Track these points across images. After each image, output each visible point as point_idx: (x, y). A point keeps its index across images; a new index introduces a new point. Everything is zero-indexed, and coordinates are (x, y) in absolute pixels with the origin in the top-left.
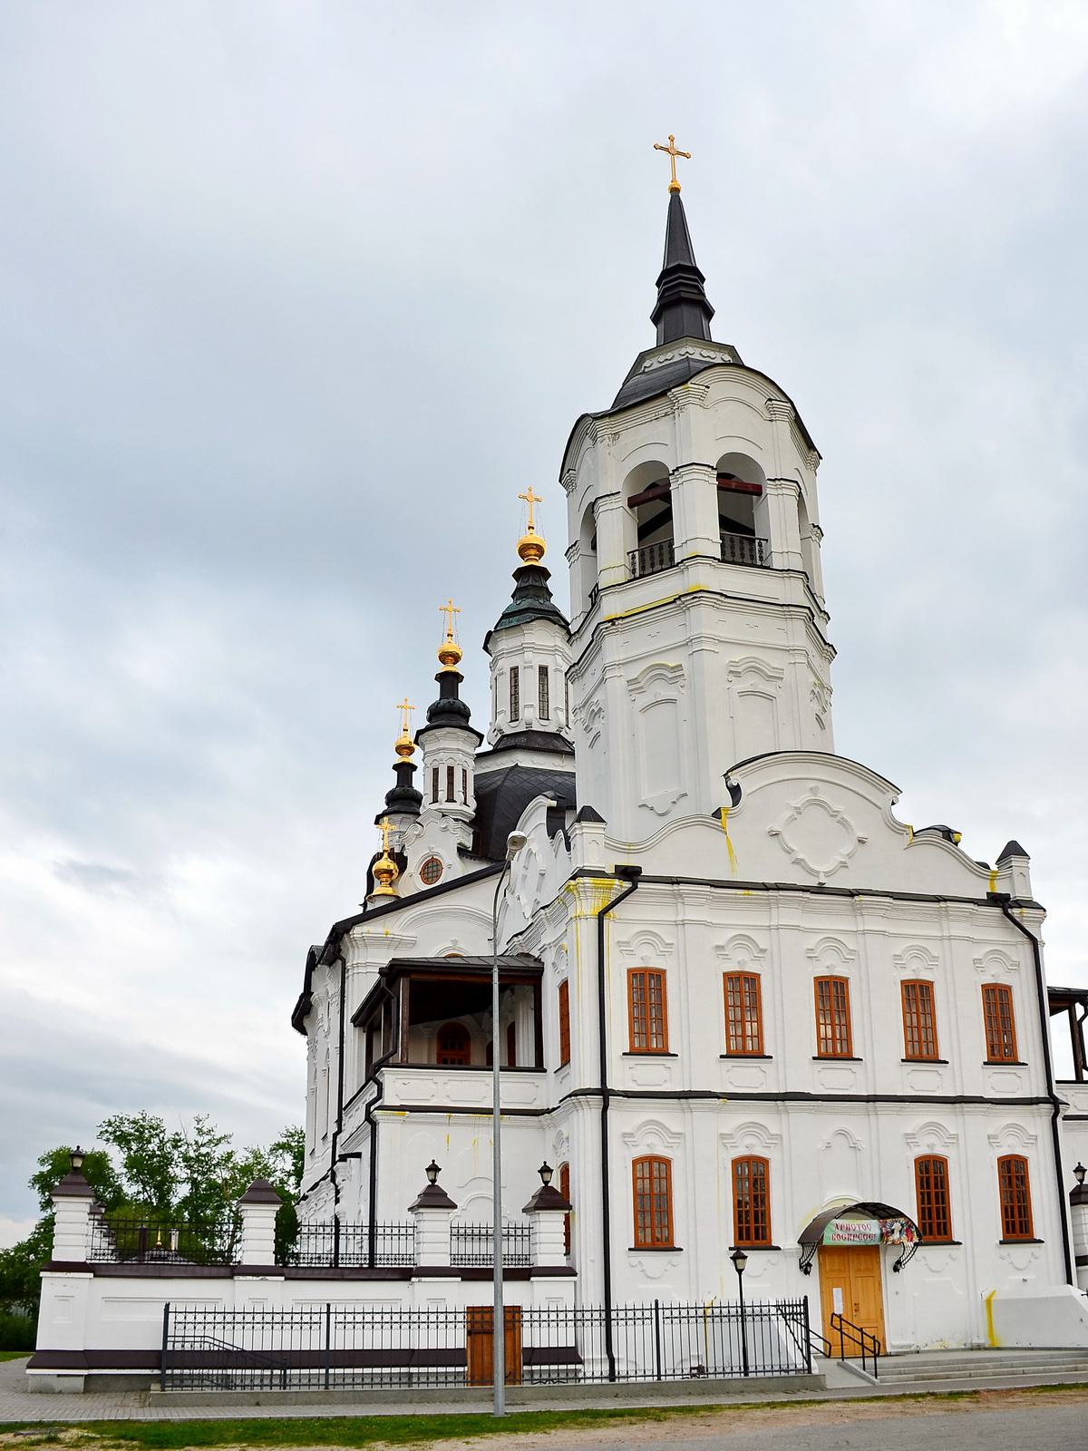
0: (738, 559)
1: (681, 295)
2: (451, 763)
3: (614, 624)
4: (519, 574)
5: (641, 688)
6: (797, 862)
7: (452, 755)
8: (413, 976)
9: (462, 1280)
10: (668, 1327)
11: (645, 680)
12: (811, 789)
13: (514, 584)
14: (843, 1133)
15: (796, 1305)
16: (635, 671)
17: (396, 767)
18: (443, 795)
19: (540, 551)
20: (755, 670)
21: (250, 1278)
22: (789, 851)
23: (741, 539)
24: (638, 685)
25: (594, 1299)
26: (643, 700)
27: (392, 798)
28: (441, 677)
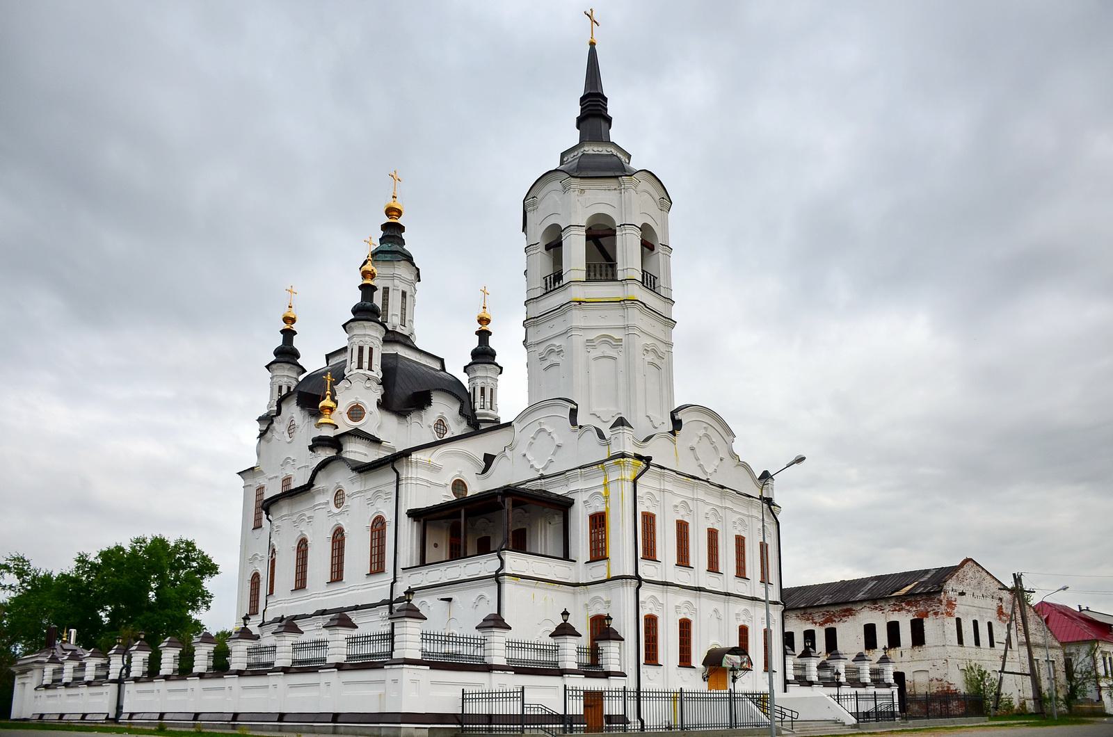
0: (598, 276)
1: (594, 111)
2: (361, 344)
3: (580, 304)
4: (385, 227)
6: (700, 466)
7: (373, 340)
8: (514, 497)
9: (586, 677)
10: (571, 701)
12: (705, 428)
16: (593, 335)
17: (283, 332)
18: (366, 365)
19: (400, 213)
20: (654, 351)
21: (499, 672)
22: (697, 459)
25: (632, 686)
26: (594, 353)
27: (278, 352)
28: (479, 333)
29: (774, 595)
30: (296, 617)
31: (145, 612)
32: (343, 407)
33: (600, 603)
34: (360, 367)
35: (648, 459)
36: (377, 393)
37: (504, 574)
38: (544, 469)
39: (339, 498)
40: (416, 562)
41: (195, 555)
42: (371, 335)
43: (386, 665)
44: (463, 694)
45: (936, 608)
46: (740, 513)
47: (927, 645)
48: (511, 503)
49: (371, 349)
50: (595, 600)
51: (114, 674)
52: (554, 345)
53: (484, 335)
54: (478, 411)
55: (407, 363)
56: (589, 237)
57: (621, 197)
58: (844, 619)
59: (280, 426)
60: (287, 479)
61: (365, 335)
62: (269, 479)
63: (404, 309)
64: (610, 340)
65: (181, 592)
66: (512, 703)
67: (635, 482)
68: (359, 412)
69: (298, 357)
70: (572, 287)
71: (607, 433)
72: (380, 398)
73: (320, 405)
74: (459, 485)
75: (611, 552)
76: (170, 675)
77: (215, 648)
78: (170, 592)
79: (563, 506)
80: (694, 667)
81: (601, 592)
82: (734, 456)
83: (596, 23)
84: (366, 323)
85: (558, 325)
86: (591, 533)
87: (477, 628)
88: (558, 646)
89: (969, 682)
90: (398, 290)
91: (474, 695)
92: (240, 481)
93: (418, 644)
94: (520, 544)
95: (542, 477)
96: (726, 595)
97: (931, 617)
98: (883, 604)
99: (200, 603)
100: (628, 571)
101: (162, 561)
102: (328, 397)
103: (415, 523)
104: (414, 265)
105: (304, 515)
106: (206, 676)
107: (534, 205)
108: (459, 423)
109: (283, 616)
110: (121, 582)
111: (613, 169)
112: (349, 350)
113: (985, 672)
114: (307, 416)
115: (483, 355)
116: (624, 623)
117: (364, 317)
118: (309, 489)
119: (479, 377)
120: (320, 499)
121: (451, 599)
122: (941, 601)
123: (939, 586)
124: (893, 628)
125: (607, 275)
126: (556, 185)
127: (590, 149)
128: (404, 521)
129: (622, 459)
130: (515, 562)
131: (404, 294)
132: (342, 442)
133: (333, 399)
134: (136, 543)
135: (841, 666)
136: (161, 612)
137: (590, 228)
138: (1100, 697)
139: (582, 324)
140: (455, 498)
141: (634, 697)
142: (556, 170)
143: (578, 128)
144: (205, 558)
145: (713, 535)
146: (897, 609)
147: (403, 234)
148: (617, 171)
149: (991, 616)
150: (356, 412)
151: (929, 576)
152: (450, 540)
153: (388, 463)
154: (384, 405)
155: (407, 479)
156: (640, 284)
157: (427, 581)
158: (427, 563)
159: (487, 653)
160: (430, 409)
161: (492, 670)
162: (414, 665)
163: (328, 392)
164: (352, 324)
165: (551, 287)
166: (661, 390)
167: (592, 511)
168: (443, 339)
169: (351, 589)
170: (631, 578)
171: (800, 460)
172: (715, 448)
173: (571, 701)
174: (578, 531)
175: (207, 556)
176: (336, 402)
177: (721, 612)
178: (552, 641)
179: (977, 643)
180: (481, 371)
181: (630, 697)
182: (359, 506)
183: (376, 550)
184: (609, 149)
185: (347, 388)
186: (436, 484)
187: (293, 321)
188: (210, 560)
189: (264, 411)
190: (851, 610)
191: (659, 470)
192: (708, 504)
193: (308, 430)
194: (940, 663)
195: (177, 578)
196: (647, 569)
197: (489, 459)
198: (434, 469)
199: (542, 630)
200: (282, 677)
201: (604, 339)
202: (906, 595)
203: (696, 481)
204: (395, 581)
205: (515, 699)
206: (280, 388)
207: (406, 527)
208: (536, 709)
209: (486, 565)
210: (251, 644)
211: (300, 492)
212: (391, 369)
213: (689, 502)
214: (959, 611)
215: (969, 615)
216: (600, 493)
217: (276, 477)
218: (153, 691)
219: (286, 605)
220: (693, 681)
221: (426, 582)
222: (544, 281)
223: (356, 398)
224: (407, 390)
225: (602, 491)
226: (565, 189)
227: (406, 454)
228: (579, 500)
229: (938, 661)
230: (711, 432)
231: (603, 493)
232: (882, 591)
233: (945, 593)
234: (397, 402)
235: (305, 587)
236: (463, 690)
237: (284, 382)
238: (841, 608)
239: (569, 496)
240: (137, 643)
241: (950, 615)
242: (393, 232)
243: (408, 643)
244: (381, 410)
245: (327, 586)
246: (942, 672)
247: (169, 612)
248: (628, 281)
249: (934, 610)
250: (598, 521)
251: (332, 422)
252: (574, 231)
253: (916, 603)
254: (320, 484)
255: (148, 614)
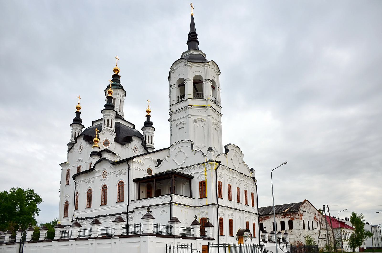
0: (197, 97)
1: (193, 39)
2: (108, 118)
3: (192, 107)
4: (113, 76)
5: (196, 122)
6: (234, 165)
7: (108, 116)
8: (175, 175)
9: (203, 240)
11: (198, 120)
13: (112, 78)
14: (248, 216)
15: (236, 245)
16: (196, 118)
17: (76, 112)
18: (110, 126)
19: (119, 71)
20: (216, 125)
21: (177, 238)
23: (198, 93)
24: (196, 121)
27: (74, 120)
29: (255, 211)
30: (99, 216)
31: (16, 216)
32: (102, 140)
33: (204, 213)
34: (108, 126)
35: (220, 162)
36: (114, 136)
37: (173, 203)
38: (181, 165)
39: (105, 174)
40: (136, 198)
41: (34, 195)
42: (111, 115)
43: (141, 236)
44: (167, 246)
45: (297, 216)
46: (246, 182)
47: (294, 229)
48: (174, 177)
49: (111, 120)
50: (202, 212)
51: (18, 240)
52: (182, 121)
53: (148, 117)
54: (147, 144)
55: (123, 126)
56: (194, 84)
57: (205, 69)
58: (266, 220)
59: (76, 147)
60: (79, 167)
61: (109, 115)
62: (72, 167)
63: (120, 106)
64: (202, 120)
65: (30, 209)
66: (170, 250)
67: (216, 170)
68: (107, 143)
69: (82, 122)
70: (189, 100)
71: (205, 153)
72: (115, 138)
73: (94, 140)
74: (149, 171)
75: (208, 195)
76: (7, 243)
77: (47, 231)
78: (26, 209)
79: (190, 178)
80: (234, 236)
81: (204, 209)
82: (243, 162)
83: (193, 8)
84: (110, 111)
85: (183, 114)
86: (200, 188)
87: (168, 222)
88: (194, 229)
89: (307, 241)
90: (119, 99)
91: (182, 246)
92: (60, 167)
93: (77, 232)
94: (172, 191)
95: (181, 168)
96: (243, 211)
97: (295, 219)
98: (279, 215)
99: (35, 213)
100: (214, 202)
101: (23, 197)
102: (97, 137)
103: (136, 184)
104: (124, 90)
105: (90, 180)
106: (60, 240)
107: (173, 71)
108: (141, 148)
109: (82, 218)
110: (7, 205)
111: (201, 59)
112: (103, 120)
113: (312, 238)
114: (87, 144)
115: (148, 124)
116: (214, 221)
117: (109, 108)
118: (93, 171)
119: (147, 132)
120: (97, 175)
121: (151, 212)
122: (299, 214)
123: (298, 209)
124: (283, 223)
125: (196, 97)
126: (182, 64)
127: (193, 52)
128: (132, 183)
129: (212, 162)
130: (176, 198)
131: (121, 101)
132: (102, 154)
133: (98, 138)
134: (12, 190)
135: (267, 235)
136: (22, 216)
137: (194, 80)
138: (343, 246)
139: (192, 114)
140: (149, 176)
141: (217, 246)
142: (180, 59)
143: (187, 44)
144: (38, 196)
145: (238, 189)
146: (284, 217)
147: (120, 79)
148: (203, 60)
149: (312, 219)
150: (106, 143)
151: (293, 206)
152: (147, 190)
153: (125, 161)
154: (116, 140)
155: (132, 167)
156: (212, 101)
157: (134, 206)
158: (140, 199)
159: (173, 231)
160: (132, 142)
161: (175, 237)
162: (152, 236)
163: (97, 135)
164: (105, 111)
165: (180, 100)
166: (218, 138)
167: (200, 180)
168: (134, 117)
169: (110, 208)
170: (216, 204)
171: (285, 163)
172: (238, 159)
173: (169, 250)
174: (195, 188)
175: (38, 195)
176: (99, 139)
177: (241, 217)
178: (191, 227)
179: (309, 229)
180: (148, 130)
181: (211, 246)
182: (114, 177)
183: (104, 194)
184: (199, 53)
185: (103, 134)
186: (142, 170)
187: (80, 109)
188: (39, 197)
189: (69, 141)
190: (268, 217)
191: (223, 166)
192: (237, 179)
193: (88, 149)
194: (298, 235)
195: (28, 203)
196: (220, 202)
197: (159, 162)
198: (142, 164)
199: (184, 223)
200: (95, 240)
201: (200, 119)
202: (287, 212)
203: (234, 171)
204: (73, 216)
205: (170, 249)
206: (75, 133)
207: (132, 185)
208: (195, 251)
209: (165, 199)
210: (62, 230)
211: (89, 172)
212: (118, 129)
213: (231, 178)
214: (304, 217)
215: (307, 219)
216: (203, 174)
217: (75, 166)
218: (36, 246)
219: (83, 214)
220: (233, 241)
221: (141, 206)
222: (177, 98)
223: (106, 138)
224: (124, 136)
225: (204, 173)
226: (186, 66)
227: (132, 158)
228: (195, 176)
229: (298, 235)
230: (237, 154)
231: (204, 174)
232: (280, 210)
233: (300, 211)
234: (120, 140)
235: (91, 207)
236: (167, 245)
237: (77, 131)
238: (265, 216)
239: (191, 175)
240: (7, 231)
241: (301, 219)
242: (116, 78)
243: (149, 227)
244: (115, 142)
245: (100, 207)
246: (299, 238)
247: (25, 216)
248: (208, 100)
249: (296, 217)
250: (203, 184)
251: (98, 146)
252: (189, 81)
253: (290, 215)
254: (97, 169)
255: (17, 217)
